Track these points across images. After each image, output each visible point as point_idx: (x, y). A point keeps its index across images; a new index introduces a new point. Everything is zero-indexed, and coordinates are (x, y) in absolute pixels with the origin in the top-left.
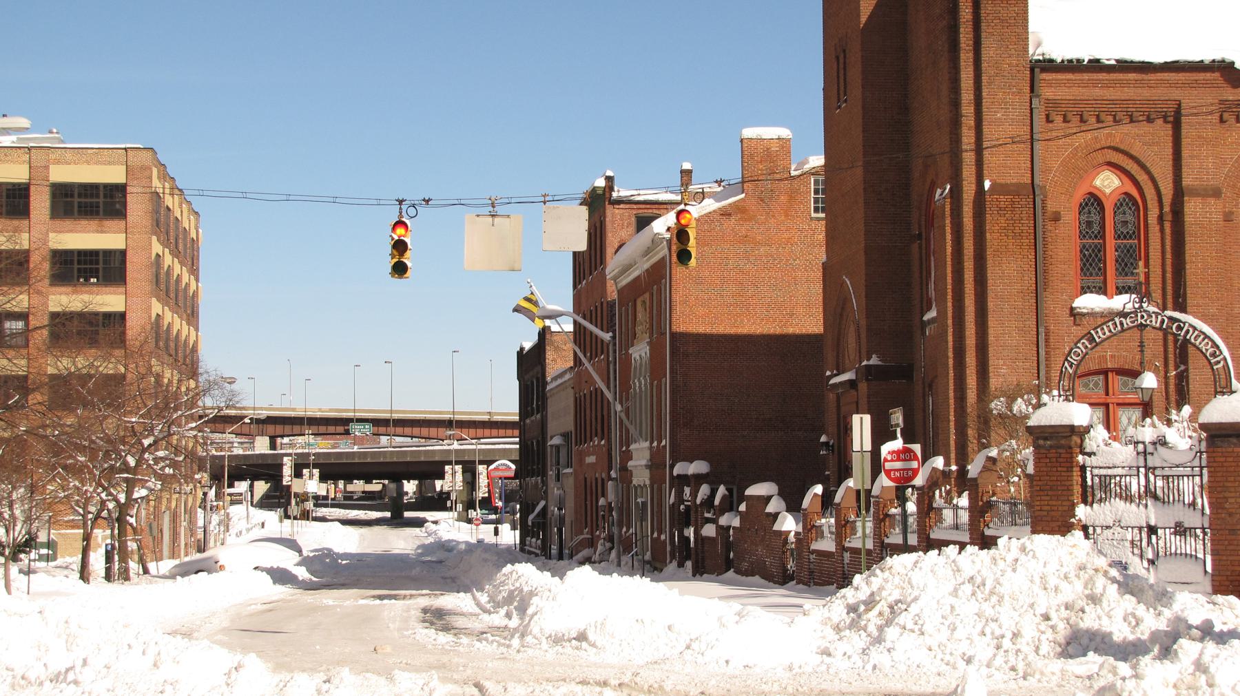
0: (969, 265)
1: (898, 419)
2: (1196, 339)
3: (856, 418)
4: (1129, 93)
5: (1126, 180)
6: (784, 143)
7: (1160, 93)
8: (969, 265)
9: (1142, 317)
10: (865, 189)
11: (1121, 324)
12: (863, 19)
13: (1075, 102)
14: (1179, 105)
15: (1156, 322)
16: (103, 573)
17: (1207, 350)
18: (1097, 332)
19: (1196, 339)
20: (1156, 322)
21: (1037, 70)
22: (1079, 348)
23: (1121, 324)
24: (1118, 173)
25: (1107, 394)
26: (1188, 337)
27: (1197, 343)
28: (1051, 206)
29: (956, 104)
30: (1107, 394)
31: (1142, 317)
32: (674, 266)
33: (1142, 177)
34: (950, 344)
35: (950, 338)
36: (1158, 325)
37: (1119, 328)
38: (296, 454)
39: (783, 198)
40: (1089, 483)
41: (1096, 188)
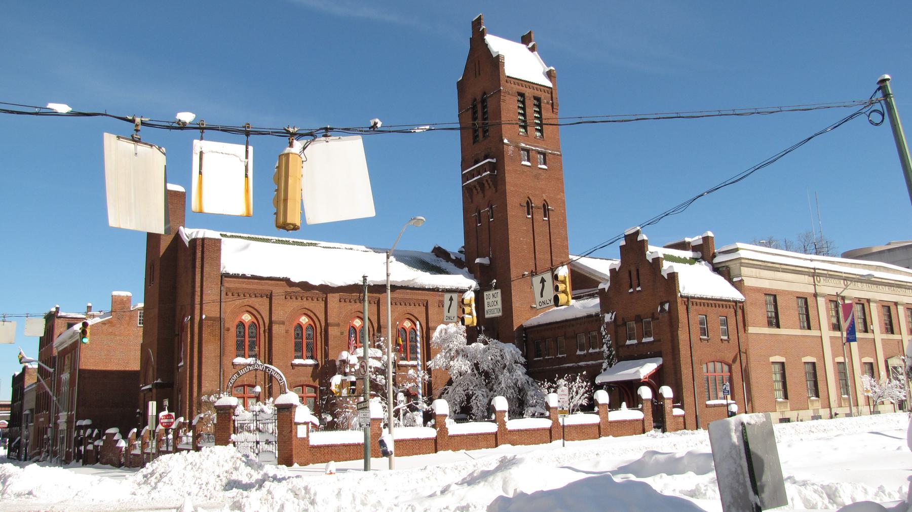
13: (237, 289)
14: (272, 292)
23: (249, 369)
29: (194, 287)
37: (248, 370)
39: (127, 318)
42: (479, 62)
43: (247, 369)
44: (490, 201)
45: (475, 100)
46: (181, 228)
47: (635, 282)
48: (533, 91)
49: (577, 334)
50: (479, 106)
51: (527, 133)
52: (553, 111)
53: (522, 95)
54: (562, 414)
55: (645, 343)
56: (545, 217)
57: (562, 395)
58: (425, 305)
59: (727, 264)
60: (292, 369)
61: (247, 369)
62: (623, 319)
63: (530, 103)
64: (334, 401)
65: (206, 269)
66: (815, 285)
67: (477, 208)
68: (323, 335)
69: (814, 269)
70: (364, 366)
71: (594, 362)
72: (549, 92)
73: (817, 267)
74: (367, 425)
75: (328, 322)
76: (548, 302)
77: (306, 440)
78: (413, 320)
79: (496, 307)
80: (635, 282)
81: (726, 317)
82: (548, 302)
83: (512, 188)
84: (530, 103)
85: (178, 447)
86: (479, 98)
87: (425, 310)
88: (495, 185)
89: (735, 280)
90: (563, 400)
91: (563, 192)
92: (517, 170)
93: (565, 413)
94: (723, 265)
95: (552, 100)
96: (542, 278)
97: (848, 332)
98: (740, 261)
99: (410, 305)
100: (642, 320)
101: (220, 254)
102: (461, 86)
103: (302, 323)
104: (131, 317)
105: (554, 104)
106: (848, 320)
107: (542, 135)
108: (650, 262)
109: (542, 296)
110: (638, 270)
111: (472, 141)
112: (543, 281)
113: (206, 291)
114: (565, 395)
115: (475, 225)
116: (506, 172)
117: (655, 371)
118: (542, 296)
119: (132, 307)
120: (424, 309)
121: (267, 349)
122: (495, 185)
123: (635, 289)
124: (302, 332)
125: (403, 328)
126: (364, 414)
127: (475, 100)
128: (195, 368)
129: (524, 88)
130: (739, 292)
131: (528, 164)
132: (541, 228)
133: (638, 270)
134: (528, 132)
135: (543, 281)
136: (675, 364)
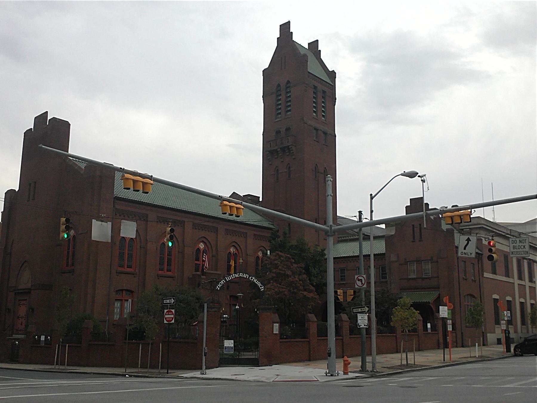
1: (366, 318)
2: (256, 282)
3: (428, 324)
5: (236, 250)
9: (241, 274)
11: (235, 276)
15: (245, 276)
16: (326, 168)
17: (259, 285)
19: (256, 282)
20: (245, 276)
22: (221, 282)
23: (235, 276)
26: (254, 281)
28: (403, 172)
29: (131, 306)
31: (241, 274)
33: (238, 248)
36: (246, 277)
37: (234, 277)
38: (532, 328)
43: (233, 276)
45: (279, 85)
53: (315, 87)
55: (160, 344)
61: (233, 276)
70: (361, 280)
74: (364, 326)
76: (469, 254)
79: (524, 250)
82: (469, 254)
84: (320, 95)
96: (469, 238)
103: (200, 248)
109: (465, 249)
112: (468, 240)
118: (465, 249)
126: (363, 316)
127: (279, 85)
134: (318, 116)
135: (468, 240)
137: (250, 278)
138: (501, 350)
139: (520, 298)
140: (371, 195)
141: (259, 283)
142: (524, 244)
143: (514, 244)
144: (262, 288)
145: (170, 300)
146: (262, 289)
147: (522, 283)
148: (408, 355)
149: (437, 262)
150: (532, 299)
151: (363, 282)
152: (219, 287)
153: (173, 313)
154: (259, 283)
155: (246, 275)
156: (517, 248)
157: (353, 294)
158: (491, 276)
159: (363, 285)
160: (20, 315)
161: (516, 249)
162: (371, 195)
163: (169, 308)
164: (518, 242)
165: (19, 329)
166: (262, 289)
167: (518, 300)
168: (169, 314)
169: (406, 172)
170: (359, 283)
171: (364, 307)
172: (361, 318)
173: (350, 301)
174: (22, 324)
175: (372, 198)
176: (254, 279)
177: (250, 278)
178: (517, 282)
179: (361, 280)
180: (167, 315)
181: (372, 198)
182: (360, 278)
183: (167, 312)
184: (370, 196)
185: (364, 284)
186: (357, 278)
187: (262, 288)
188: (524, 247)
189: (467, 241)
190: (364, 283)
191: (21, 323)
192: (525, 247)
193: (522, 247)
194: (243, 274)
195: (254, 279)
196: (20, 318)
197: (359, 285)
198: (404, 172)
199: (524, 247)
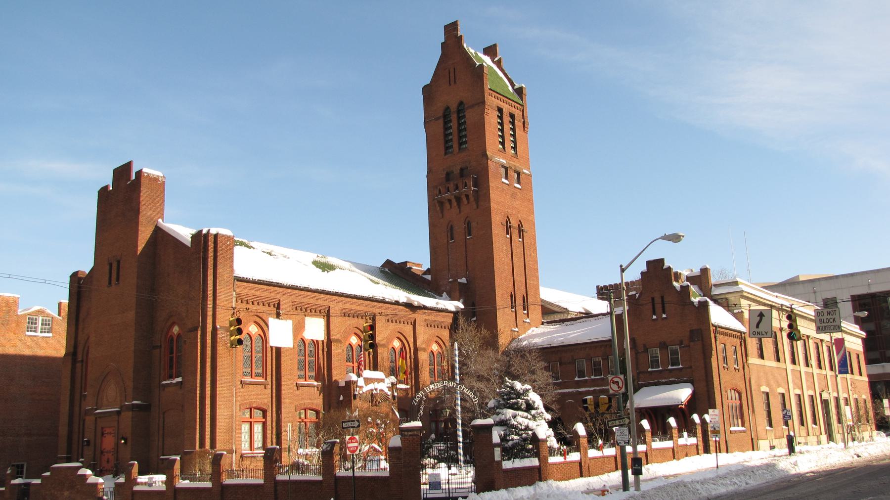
0: (208, 361)
4: (263, 294)
6: (18, 298)
7: (273, 295)
8: (208, 361)
9: (446, 383)
10: (135, 323)
12: (140, 249)
13: (247, 295)
14: (280, 301)
18: (427, 389)
19: (467, 391)
21: (235, 280)
24: (257, 326)
25: (251, 418)
27: (468, 393)
29: (205, 291)
30: (251, 418)
31: (446, 383)
32: (221, 349)
34: (198, 395)
35: (198, 392)
39: (14, 325)
40: (740, 420)
41: (250, 331)
42: (454, 69)
44: (467, 217)
46: (160, 220)
47: (658, 307)
48: (509, 106)
49: (575, 360)
50: (454, 117)
51: (505, 150)
52: (524, 130)
54: (714, 433)
56: (520, 238)
57: (713, 415)
58: (413, 324)
59: (727, 296)
60: (297, 390)
62: (645, 346)
63: (507, 119)
64: (450, 426)
65: (220, 270)
66: (780, 320)
67: (448, 224)
68: (325, 353)
69: (782, 305)
70: (618, 382)
71: (604, 388)
72: (521, 110)
73: (783, 304)
74: (625, 443)
75: (331, 338)
77: (500, 463)
78: (402, 339)
80: (658, 307)
81: (725, 345)
83: (495, 206)
84: (507, 119)
85: (277, 479)
86: (454, 107)
87: (412, 329)
88: (477, 200)
89: (736, 311)
90: (714, 420)
91: (533, 214)
92: (498, 188)
93: (717, 433)
94: (723, 297)
95: (523, 118)
97: (840, 364)
98: (741, 294)
99: (400, 323)
100: (667, 347)
101: (233, 254)
102: (428, 92)
104: (18, 323)
105: (526, 123)
106: (840, 354)
107: (516, 153)
108: (677, 291)
110: (662, 298)
111: (443, 153)
113: (220, 296)
114: (716, 415)
115: (445, 241)
116: (490, 188)
117: (690, 396)
119: (19, 310)
120: (411, 327)
121: (274, 366)
122: (477, 200)
123: (659, 317)
124: (305, 348)
125: (393, 347)
126: (622, 431)
127: (448, 108)
128: (207, 386)
129: (501, 103)
130: (740, 323)
131: (506, 182)
132: (517, 249)
133: (662, 298)
136: (708, 391)
137: (458, 387)
138: (751, 471)
139: (794, 388)
140: (621, 266)
141: (471, 394)
142: (834, 317)
143: (821, 317)
144: (476, 399)
145: (352, 423)
146: (476, 401)
147: (809, 370)
148: (352, 475)
149: (689, 346)
150: (810, 389)
151: (620, 385)
152: (416, 401)
153: (357, 441)
154: (471, 394)
155: (453, 383)
156: (825, 322)
157: (608, 402)
158: (759, 361)
159: (621, 389)
160: (105, 449)
161: (824, 323)
162: (621, 266)
163: (352, 433)
164: (825, 313)
165: (105, 469)
166: (476, 401)
167: (794, 391)
168: (352, 443)
169: (667, 234)
170: (615, 387)
171: (624, 418)
172: (619, 434)
173: (603, 411)
174: (108, 462)
175: (623, 270)
176: (464, 389)
177: (458, 387)
178: (790, 366)
179: (618, 382)
180: (350, 443)
181: (623, 270)
182: (616, 380)
183: (349, 439)
184: (619, 268)
185: (621, 388)
186: (612, 380)
187: (476, 399)
188: (834, 320)
189: (759, 317)
190: (621, 386)
191: (106, 460)
192: (835, 319)
193: (832, 320)
194: (449, 383)
195: (464, 389)
196: (106, 453)
197: (615, 390)
198: (665, 234)
199: (834, 320)
